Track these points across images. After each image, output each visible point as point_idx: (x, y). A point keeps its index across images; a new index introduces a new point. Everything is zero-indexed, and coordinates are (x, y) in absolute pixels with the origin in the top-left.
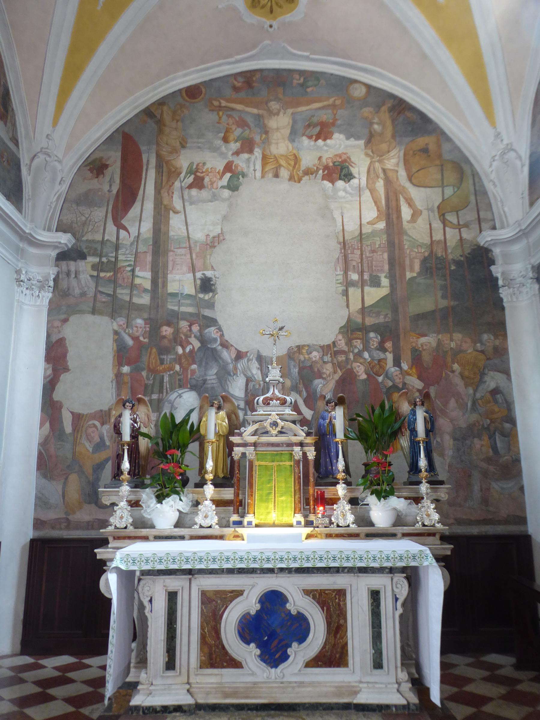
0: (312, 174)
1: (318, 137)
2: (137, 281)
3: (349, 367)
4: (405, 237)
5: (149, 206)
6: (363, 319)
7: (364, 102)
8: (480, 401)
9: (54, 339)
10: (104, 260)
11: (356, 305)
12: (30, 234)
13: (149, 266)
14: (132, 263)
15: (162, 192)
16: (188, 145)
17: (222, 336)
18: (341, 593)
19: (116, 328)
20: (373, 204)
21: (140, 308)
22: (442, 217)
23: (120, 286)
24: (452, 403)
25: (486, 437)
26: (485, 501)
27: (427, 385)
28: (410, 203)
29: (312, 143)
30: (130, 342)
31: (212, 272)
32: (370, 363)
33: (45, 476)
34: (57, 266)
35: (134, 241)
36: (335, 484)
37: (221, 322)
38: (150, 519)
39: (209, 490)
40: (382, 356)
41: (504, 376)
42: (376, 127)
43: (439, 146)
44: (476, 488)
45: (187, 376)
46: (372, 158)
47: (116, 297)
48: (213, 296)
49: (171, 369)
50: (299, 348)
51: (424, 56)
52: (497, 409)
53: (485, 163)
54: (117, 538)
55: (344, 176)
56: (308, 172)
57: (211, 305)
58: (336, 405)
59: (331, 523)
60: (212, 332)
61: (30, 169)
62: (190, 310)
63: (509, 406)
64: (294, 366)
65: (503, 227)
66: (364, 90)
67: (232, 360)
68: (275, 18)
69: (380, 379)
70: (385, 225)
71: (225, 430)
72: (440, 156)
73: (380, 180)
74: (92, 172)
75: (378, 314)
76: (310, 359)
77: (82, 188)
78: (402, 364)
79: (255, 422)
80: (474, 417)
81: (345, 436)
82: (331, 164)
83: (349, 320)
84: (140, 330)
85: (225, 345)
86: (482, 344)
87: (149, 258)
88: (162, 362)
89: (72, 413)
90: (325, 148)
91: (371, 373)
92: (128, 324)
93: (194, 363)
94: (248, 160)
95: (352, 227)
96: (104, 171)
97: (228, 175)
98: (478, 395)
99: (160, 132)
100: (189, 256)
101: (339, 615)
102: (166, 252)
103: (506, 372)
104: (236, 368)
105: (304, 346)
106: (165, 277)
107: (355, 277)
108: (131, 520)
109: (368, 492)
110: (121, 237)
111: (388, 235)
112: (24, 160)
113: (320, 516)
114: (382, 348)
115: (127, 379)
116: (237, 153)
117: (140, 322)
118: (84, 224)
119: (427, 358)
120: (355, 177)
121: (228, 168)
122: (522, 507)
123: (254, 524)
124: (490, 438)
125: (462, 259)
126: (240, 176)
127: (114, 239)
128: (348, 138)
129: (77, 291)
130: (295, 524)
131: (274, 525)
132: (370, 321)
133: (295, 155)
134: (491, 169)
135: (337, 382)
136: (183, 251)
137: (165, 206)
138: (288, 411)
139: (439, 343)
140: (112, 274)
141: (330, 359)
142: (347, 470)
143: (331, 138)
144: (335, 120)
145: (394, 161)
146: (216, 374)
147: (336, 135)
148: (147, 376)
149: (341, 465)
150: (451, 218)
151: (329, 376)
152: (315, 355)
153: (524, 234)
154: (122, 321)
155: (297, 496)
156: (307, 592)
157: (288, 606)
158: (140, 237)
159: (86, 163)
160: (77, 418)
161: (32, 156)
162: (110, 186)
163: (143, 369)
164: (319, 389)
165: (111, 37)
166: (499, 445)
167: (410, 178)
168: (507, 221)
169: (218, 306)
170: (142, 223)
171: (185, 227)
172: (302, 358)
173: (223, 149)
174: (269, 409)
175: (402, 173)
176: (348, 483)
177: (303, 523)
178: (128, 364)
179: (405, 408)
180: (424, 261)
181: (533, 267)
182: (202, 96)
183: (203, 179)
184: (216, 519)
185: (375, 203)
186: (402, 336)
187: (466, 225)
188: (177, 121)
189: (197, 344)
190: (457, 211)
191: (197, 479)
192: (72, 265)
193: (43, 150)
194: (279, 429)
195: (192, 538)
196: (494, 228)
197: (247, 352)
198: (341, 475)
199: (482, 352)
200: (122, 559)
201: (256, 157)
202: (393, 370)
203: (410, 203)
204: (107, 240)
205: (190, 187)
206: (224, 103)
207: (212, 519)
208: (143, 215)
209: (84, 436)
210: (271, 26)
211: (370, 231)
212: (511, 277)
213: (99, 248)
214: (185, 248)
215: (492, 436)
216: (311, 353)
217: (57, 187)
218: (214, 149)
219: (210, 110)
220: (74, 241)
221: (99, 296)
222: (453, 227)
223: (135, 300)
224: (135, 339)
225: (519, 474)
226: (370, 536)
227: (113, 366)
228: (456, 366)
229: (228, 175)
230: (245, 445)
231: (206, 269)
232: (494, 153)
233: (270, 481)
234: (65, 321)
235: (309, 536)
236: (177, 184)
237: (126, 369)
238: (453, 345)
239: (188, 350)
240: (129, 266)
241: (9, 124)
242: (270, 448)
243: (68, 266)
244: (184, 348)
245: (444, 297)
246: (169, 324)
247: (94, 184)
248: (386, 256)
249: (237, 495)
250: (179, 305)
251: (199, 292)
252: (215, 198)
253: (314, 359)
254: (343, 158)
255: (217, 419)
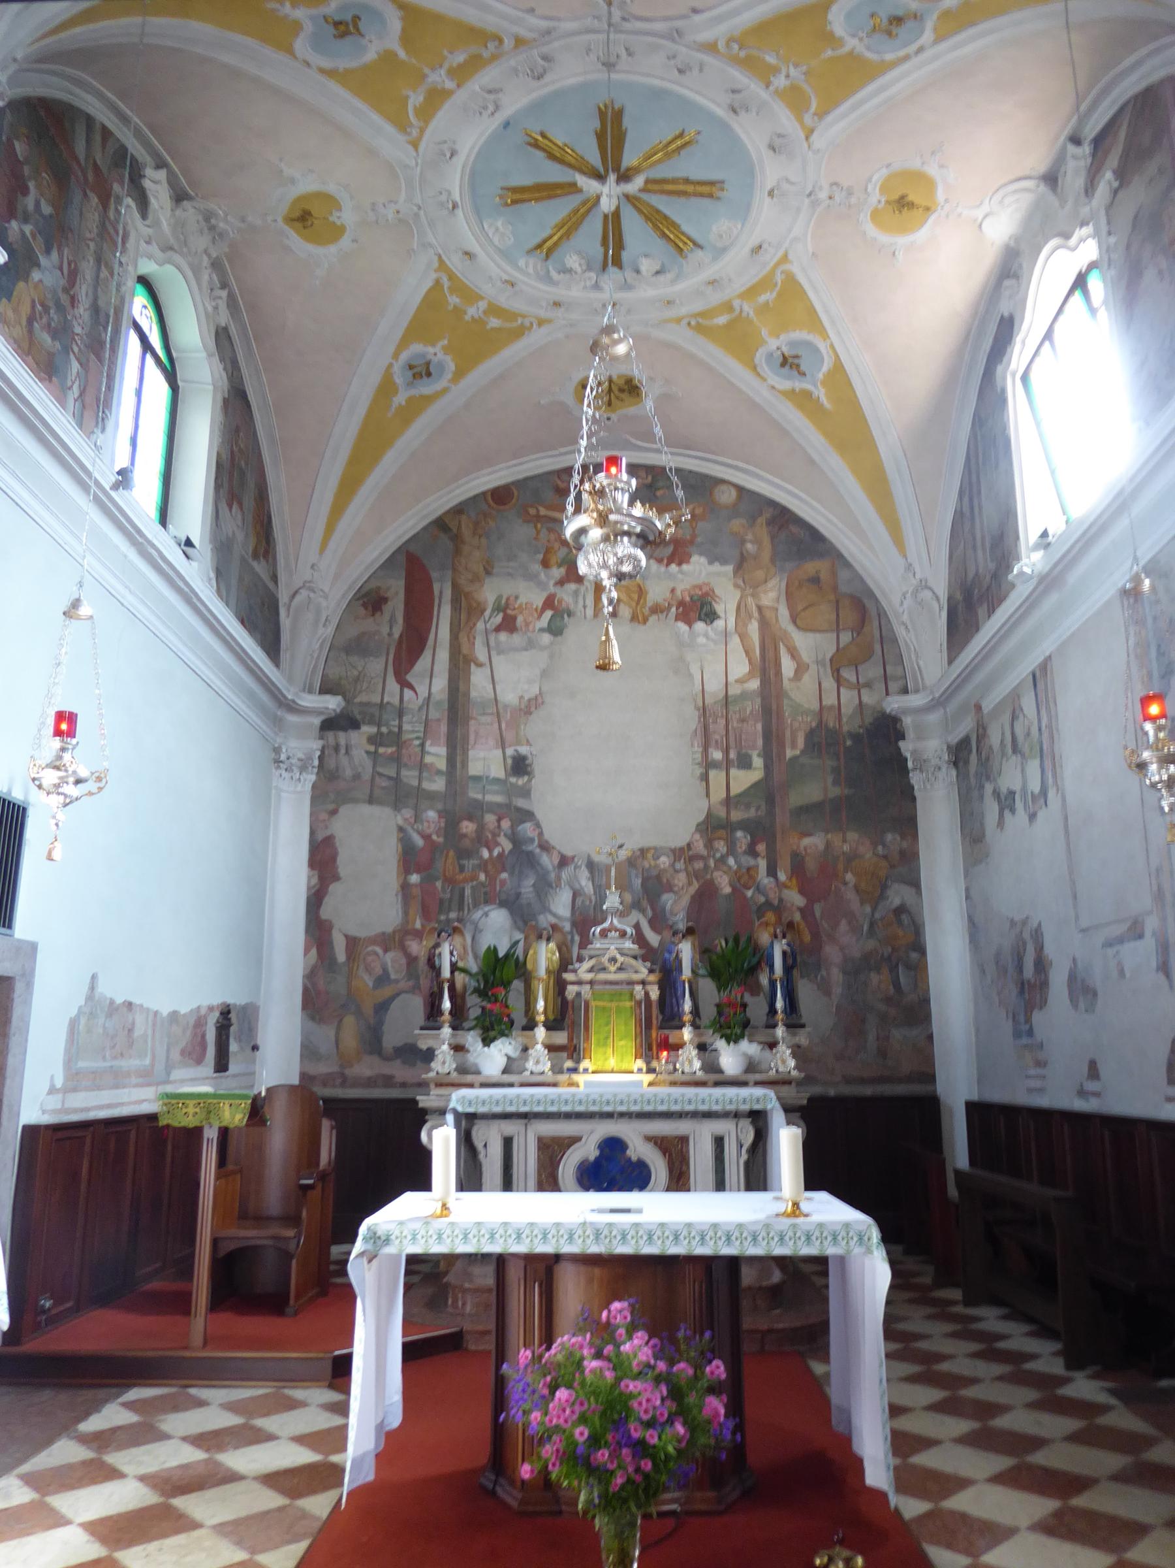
0: (662, 612)
1: (670, 561)
2: (428, 759)
3: (709, 877)
4: (786, 702)
5: (443, 655)
6: (728, 813)
7: (734, 511)
8: (880, 924)
9: (320, 837)
10: (384, 730)
11: (718, 794)
12: (294, 701)
13: (443, 739)
14: (421, 735)
15: (461, 635)
16: (495, 571)
17: (541, 834)
18: (684, 1140)
19: (400, 822)
20: (744, 655)
21: (431, 796)
22: (835, 674)
23: (406, 765)
24: (843, 926)
25: (885, 971)
26: (882, 1053)
27: (811, 902)
28: (794, 653)
29: (663, 569)
30: (419, 842)
31: (528, 748)
32: (736, 873)
33: (313, 1018)
34: (321, 738)
35: (423, 705)
36: (681, 1027)
37: (539, 815)
38: (476, 1065)
39: (540, 1032)
40: (752, 862)
41: (913, 891)
42: (749, 546)
43: (834, 574)
44: (871, 1037)
45: (495, 890)
46: (743, 590)
47: (401, 780)
48: (530, 781)
49: (474, 878)
50: (643, 852)
51: (812, 462)
52: (900, 933)
53: (896, 599)
54: (440, 1085)
55: (706, 615)
56: (657, 610)
57: (526, 793)
58: (684, 936)
59: (675, 1070)
60: (527, 829)
61: (288, 610)
62: (499, 799)
63: (917, 931)
64: (637, 876)
65: (917, 691)
66: (734, 493)
67: (554, 867)
68: (614, 411)
69: (749, 893)
70: (759, 683)
71: (555, 965)
72: (835, 588)
73: (753, 621)
74: (366, 609)
75: (748, 806)
76: (657, 866)
77: (352, 632)
78: (779, 874)
79: (591, 957)
80: (871, 944)
81: (693, 971)
82: (688, 599)
83: (709, 815)
84: (433, 826)
85: (545, 847)
86: (884, 845)
87: (444, 728)
88: (462, 869)
89: (346, 936)
90: (680, 576)
91: (738, 885)
92: (417, 818)
93: (504, 870)
94: (576, 593)
95: (714, 687)
96: (383, 607)
97: (549, 614)
98: (877, 916)
99: (457, 552)
100: (496, 725)
101: (681, 1162)
102: (467, 719)
103: (916, 884)
104: (559, 878)
105: (648, 849)
106: (465, 752)
107: (717, 755)
108: (454, 1066)
109: (717, 1035)
110: (406, 698)
111: (763, 699)
112: (283, 597)
113: (664, 1061)
114: (752, 852)
115: (417, 892)
116: (561, 583)
117: (432, 814)
118: (357, 680)
119: (811, 865)
120: (719, 617)
121: (549, 603)
122: (929, 1060)
123: (590, 1070)
124: (891, 971)
125: (861, 731)
126: (566, 616)
127: (396, 701)
128: (711, 562)
129: (348, 773)
130: (635, 1070)
131: (612, 1072)
132: (736, 815)
133: (639, 586)
134: (901, 610)
135: (693, 898)
136: (488, 719)
137: (464, 656)
138: (628, 945)
139: (828, 845)
140: (394, 749)
141: (683, 867)
142: (696, 1012)
143: (688, 562)
144: (694, 536)
145: (772, 595)
146: (534, 885)
147: (695, 558)
148: (443, 887)
149: (687, 1006)
150: (848, 674)
151: (683, 888)
152: (664, 861)
153: (937, 704)
154: (408, 813)
155: (638, 1040)
156: (649, 1139)
157: (628, 1152)
158: (432, 699)
159: (358, 596)
160: (353, 943)
161: (292, 593)
162: (391, 628)
163: (437, 879)
164: (668, 907)
165: (400, 443)
166: (902, 979)
167: (794, 619)
168: (922, 679)
169: (535, 795)
170: (434, 680)
171: (491, 686)
172: (646, 865)
173: (542, 575)
174: (606, 941)
175: (784, 612)
176: (695, 1026)
177: (645, 1069)
178: (418, 871)
179: (764, 938)
180: (810, 734)
181: (949, 747)
182: (514, 500)
183: (514, 618)
184: (549, 1064)
185: (747, 653)
186: (779, 836)
187: (868, 685)
188: (480, 537)
189: (507, 846)
190: (855, 664)
191: (524, 1021)
192: (342, 737)
193: (308, 585)
194: (618, 965)
195: (522, 1085)
196: (905, 691)
197: (573, 858)
198: (687, 1018)
199: (885, 857)
200: (458, 1101)
201: (587, 588)
202: (766, 881)
203: (794, 653)
204: (388, 703)
205: (498, 629)
206: (543, 512)
207: (545, 1064)
208: (436, 668)
209: (362, 967)
210: (609, 419)
211: (739, 692)
212: (925, 757)
213: (377, 714)
214: (492, 714)
215: (894, 969)
216: (658, 858)
217: (321, 630)
218: (531, 577)
219: (524, 521)
220: (343, 704)
221: (378, 780)
222: (850, 686)
223: (426, 785)
224: (427, 837)
225: (927, 1018)
226: (717, 1084)
227: (398, 874)
228: (849, 877)
229: (549, 614)
230: (579, 983)
231: (518, 743)
232: (904, 589)
233: (608, 1024)
234: (334, 812)
235: (650, 1084)
236: (480, 625)
237: (414, 878)
238: (846, 848)
239: (495, 853)
240: (418, 738)
241: (270, 560)
242: (608, 987)
243: (336, 737)
244: (490, 851)
245: (836, 782)
246: (470, 818)
247: (368, 624)
248: (759, 726)
249: (571, 1039)
250: (484, 791)
251: (510, 775)
252: (531, 645)
253: (662, 866)
254: (704, 591)
255: (547, 952)
